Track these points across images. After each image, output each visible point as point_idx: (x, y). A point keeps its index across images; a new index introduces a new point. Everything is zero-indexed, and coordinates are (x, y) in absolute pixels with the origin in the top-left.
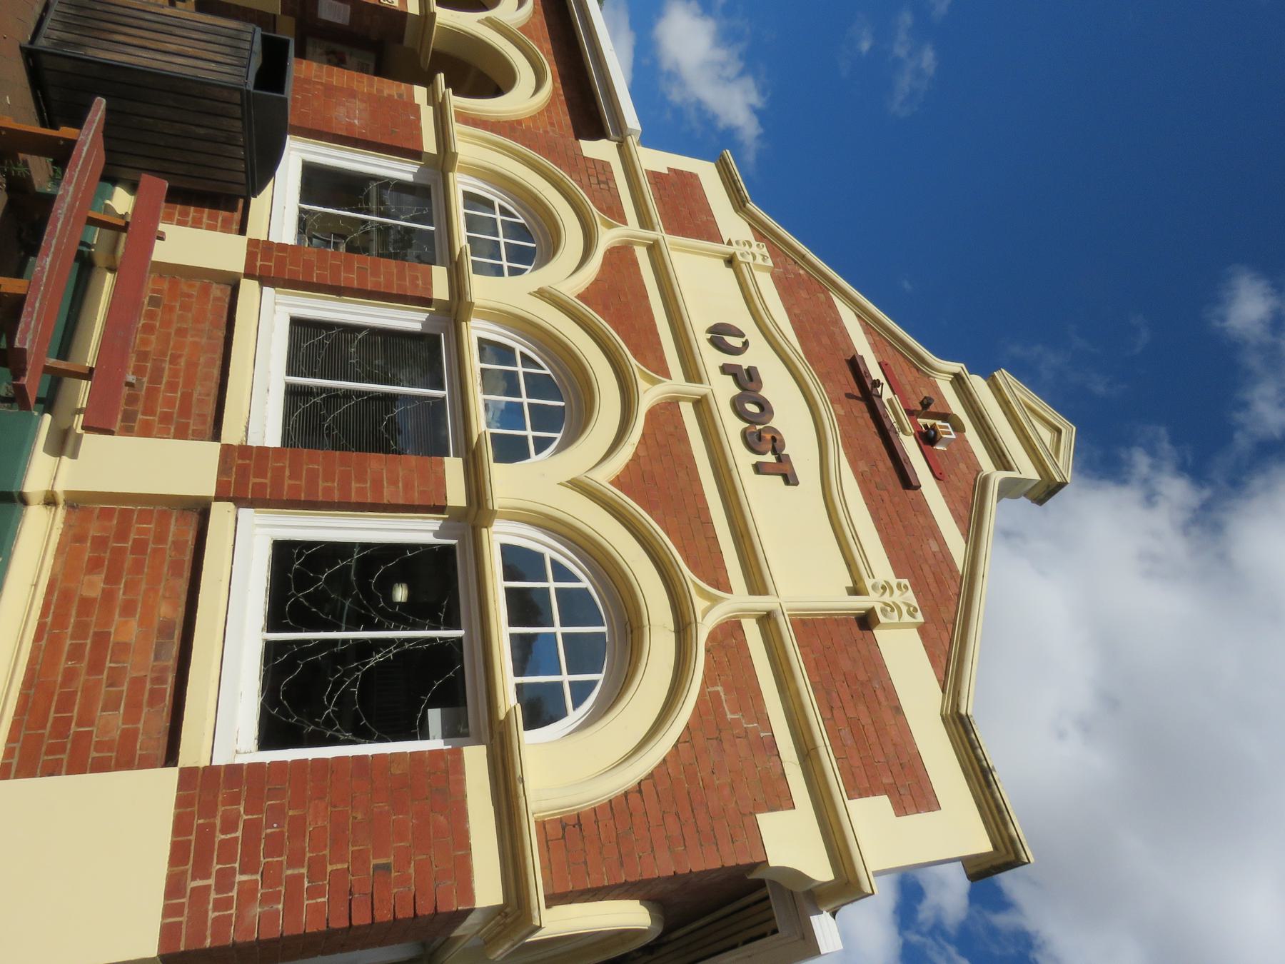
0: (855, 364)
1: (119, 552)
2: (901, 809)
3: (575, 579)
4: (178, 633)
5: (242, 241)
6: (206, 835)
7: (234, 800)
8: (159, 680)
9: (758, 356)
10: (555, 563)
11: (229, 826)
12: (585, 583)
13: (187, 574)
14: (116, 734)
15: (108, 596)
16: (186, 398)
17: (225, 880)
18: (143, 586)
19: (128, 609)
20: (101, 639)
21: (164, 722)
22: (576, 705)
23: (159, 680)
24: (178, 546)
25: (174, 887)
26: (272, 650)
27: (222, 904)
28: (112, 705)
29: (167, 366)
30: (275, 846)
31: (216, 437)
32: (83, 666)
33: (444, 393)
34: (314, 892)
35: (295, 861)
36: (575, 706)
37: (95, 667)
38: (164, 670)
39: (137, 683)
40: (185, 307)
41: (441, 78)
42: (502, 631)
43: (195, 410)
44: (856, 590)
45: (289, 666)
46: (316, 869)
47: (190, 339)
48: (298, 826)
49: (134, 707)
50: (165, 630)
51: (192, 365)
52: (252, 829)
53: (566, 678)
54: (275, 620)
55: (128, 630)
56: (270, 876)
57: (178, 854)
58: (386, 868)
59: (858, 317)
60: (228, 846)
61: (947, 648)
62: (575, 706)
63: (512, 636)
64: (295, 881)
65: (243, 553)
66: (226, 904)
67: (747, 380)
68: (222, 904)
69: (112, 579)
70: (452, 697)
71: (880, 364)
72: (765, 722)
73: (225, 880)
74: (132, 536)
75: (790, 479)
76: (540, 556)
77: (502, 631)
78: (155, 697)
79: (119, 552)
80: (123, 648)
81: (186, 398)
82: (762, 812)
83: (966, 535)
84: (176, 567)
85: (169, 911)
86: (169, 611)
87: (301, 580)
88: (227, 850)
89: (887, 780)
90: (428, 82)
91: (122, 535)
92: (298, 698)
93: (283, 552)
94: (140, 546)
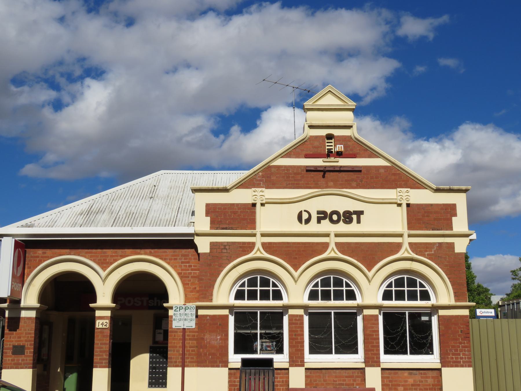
0: (310, 170)
1: (392, 385)
2: (455, 215)
3: (245, 282)
4: (411, 371)
5: (291, 369)
6: (454, 362)
7: (448, 358)
8: (421, 374)
9: (314, 206)
10: (240, 287)
11: (452, 358)
12: (319, 280)
13: (397, 371)
14: (432, 380)
15: (403, 385)
16: (347, 377)
17: (462, 358)
18: (400, 379)
19: (406, 381)
20: (412, 385)
21: (430, 372)
22: (278, 287)
23: (421, 374)
24: (390, 374)
25: (462, 366)
26: (411, 353)
27: (465, 358)
28: (427, 381)
29: (337, 383)
30: (456, 350)
31: (288, 369)
32: (418, 387)
33: (407, 312)
34: (464, 343)
35: (459, 347)
36: (278, 287)
37: (419, 385)
38: (419, 373)
39: (422, 377)
40: (316, 381)
41: (91, 305)
42: (333, 303)
43: (351, 374)
44: (400, 205)
45: (414, 349)
46: (460, 343)
47: (327, 378)
48: (453, 347)
49: (427, 377)
50: (410, 374)
51: (336, 377)
52: (453, 354)
53: (271, 288)
54: (405, 353)
55: (411, 381)
56: (461, 351)
57: (457, 366)
58: (461, 331)
59: (282, 157)
60: (456, 358)
61: (414, 183)
62: (278, 287)
63: (248, 300)
64: (463, 347)
65: (389, 360)
66: (465, 358)
67: (322, 216)
68: (465, 358)
69: (399, 385)
70: (420, 315)
71: (306, 158)
72: (434, 244)
73: (462, 358)
74: (388, 383)
75: (362, 213)
76: (385, 291)
77: (258, 303)
78: (425, 374)
79: (392, 385)
80: (414, 381)
81: (347, 377)
82: (454, 251)
83: (378, 157)
84: (395, 374)
85: (466, 366)
86: (406, 373)
87: (394, 347)
88: (457, 358)
89: (449, 216)
90: (93, 310)
91: (388, 385)
92: (423, 346)
93: (386, 352)
94: (390, 381)
